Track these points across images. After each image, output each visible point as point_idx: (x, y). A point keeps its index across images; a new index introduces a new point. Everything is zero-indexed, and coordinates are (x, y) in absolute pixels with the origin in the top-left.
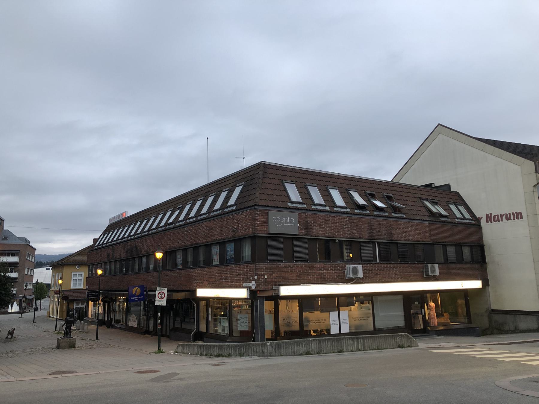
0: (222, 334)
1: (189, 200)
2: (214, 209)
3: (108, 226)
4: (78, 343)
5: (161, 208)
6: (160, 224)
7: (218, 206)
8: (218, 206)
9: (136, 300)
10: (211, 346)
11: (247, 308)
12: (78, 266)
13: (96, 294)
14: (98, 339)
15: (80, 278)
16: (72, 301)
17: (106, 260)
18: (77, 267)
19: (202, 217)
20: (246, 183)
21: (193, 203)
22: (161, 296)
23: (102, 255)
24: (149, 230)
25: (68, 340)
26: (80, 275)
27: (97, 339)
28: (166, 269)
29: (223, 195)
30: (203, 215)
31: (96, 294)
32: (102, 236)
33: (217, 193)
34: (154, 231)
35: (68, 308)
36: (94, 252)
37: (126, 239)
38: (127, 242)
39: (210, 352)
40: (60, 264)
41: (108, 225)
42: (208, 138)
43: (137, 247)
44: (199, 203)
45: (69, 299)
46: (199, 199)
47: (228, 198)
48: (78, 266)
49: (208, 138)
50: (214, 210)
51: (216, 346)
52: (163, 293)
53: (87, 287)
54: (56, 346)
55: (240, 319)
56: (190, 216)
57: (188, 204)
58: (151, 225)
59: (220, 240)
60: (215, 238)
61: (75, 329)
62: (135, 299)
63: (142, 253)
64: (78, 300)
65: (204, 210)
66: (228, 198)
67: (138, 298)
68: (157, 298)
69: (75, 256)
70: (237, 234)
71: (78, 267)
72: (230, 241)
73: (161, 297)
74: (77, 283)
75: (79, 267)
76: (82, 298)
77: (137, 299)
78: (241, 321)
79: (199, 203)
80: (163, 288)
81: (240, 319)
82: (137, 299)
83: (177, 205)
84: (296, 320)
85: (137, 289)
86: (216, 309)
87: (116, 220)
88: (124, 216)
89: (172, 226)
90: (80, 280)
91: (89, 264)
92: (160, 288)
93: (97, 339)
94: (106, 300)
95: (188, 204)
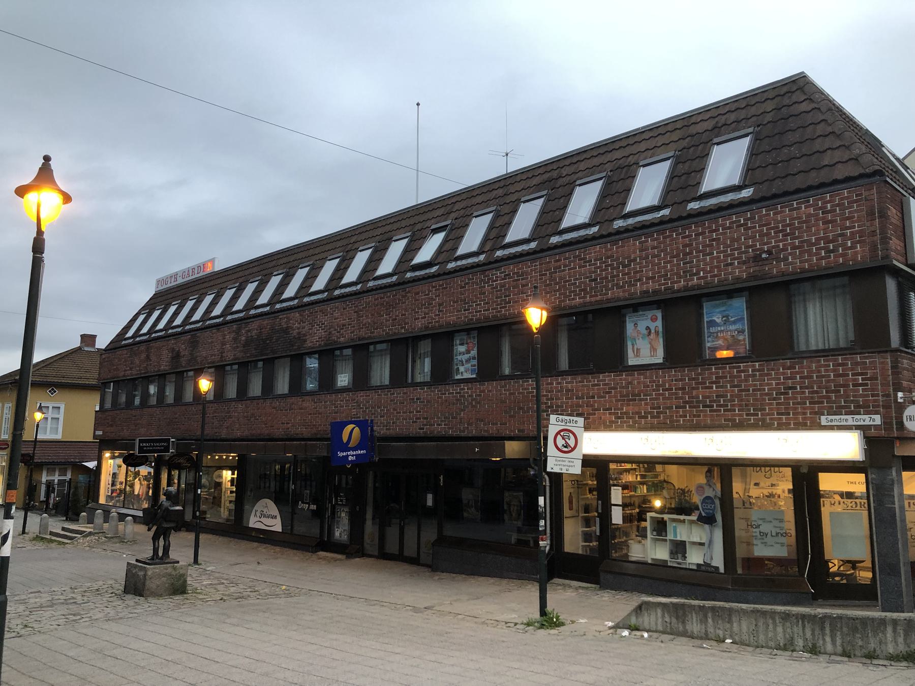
0: (669, 564)
1: (174, 298)
2: (506, 241)
3: (154, 295)
4: (193, 578)
5: (211, 283)
6: (174, 321)
7: (240, 305)
8: (240, 305)
9: (350, 458)
10: (864, 621)
11: (645, 492)
12: (53, 389)
13: (160, 446)
14: (199, 562)
15: (57, 416)
16: (40, 466)
17: (167, 368)
18: (50, 391)
19: (142, 338)
20: (378, 244)
21: (149, 312)
22: (563, 442)
23: (153, 358)
24: (166, 328)
25: (170, 570)
26: (56, 410)
27: (196, 561)
28: (406, 381)
29: (251, 288)
30: (213, 319)
31: (160, 446)
32: (142, 318)
33: (378, 244)
34: (144, 338)
35: (31, 480)
36: (125, 352)
37: (131, 341)
38: (248, 321)
39: (860, 643)
40: (11, 383)
41: (154, 293)
42: (418, 104)
43: (286, 331)
44: (208, 299)
45: (35, 461)
46: (190, 298)
47: (213, 304)
48: (53, 389)
49: (418, 104)
50: (257, 306)
51: (895, 622)
52: (571, 434)
53: (100, 433)
54: (122, 588)
55: (760, 522)
56: (175, 324)
57: (359, 249)
58: (207, 309)
59: (673, 292)
60: (651, 286)
61: (90, 532)
62: (348, 456)
63: (308, 344)
64: (53, 463)
65: (217, 311)
66: (213, 304)
67: (354, 453)
68: (551, 450)
69: (48, 365)
70: (775, 269)
71: (53, 391)
72: (727, 293)
73: (565, 447)
74: (49, 426)
75: (55, 392)
76: (63, 461)
77: (353, 456)
78: (762, 529)
79: (208, 299)
80: (572, 418)
81: (760, 522)
82: (353, 456)
83: (474, 208)
84: (786, 528)
85: (354, 428)
86: (590, 493)
87: (180, 281)
88: (209, 270)
89: (434, 269)
90: (54, 421)
91: (104, 379)
92: (561, 417)
93: (196, 561)
94: (179, 461)
95: (359, 249)
